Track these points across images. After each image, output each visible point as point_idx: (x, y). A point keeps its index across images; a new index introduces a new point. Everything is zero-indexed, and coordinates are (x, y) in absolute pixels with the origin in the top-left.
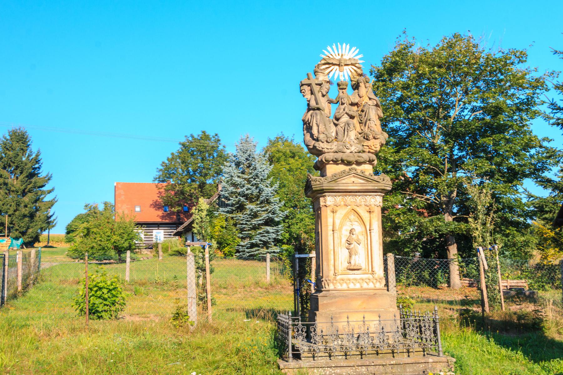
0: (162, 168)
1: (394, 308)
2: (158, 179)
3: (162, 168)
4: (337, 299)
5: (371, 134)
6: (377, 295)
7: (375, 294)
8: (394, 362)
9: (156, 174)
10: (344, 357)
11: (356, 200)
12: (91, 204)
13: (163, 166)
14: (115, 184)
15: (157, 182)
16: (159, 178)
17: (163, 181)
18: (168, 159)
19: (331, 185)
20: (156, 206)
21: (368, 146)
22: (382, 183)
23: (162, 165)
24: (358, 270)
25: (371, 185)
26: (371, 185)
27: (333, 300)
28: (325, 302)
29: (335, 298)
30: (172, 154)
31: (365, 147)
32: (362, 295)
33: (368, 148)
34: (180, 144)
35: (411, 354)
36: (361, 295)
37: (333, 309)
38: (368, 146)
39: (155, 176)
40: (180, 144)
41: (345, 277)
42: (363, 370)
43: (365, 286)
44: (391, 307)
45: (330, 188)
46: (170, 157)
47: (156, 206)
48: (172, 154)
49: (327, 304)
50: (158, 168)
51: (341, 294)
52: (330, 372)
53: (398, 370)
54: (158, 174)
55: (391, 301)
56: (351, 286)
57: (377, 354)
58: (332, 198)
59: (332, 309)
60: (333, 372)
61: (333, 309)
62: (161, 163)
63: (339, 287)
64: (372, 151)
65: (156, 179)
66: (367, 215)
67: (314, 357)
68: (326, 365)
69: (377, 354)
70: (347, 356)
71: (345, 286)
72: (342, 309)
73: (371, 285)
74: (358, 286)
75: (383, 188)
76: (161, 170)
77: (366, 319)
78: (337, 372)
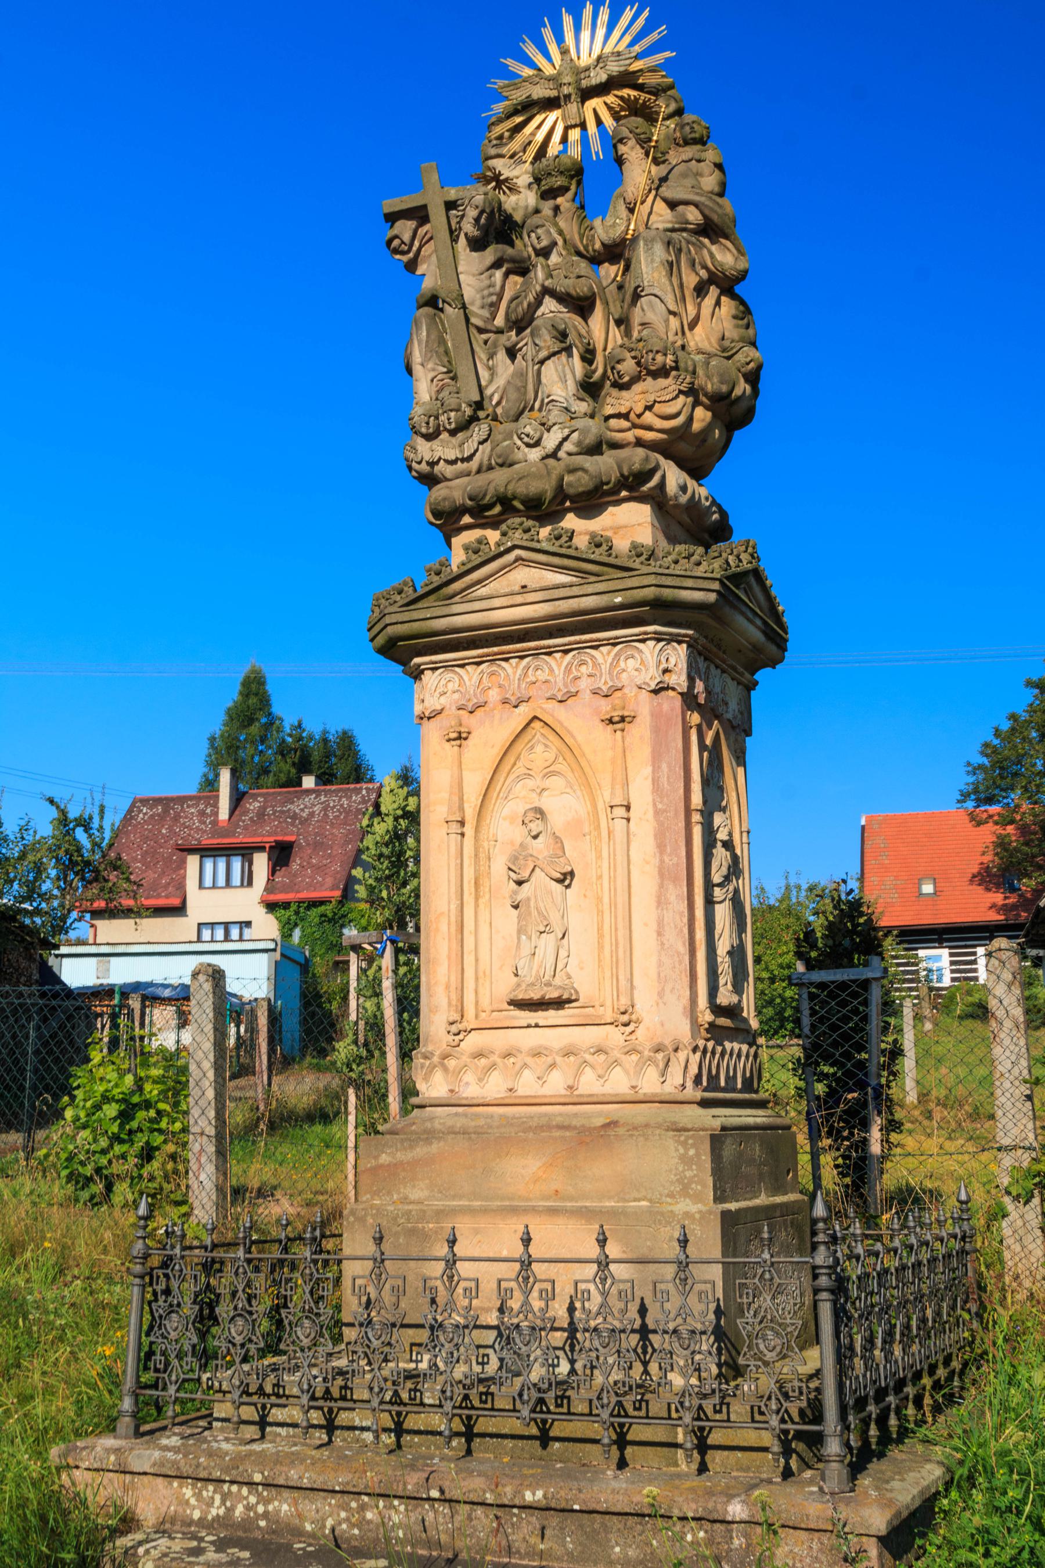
0: (985, 761)
1: (697, 1198)
2: (973, 797)
3: (985, 761)
4: (435, 1148)
5: (628, 355)
6: (621, 1131)
7: (612, 1124)
8: (539, 1494)
9: (964, 780)
10: (388, 1439)
11: (552, 670)
12: (823, 883)
13: (987, 756)
14: (863, 822)
15: (970, 804)
16: (976, 791)
17: (990, 800)
18: (997, 733)
19: (415, 615)
20: (986, 878)
21: (626, 416)
22: (645, 569)
23: (983, 754)
24: (559, 1003)
25: (590, 589)
26: (590, 589)
27: (420, 1151)
28: (384, 1159)
29: (428, 1141)
30: (1013, 717)
31: (613, 422)
32: (549, 1127)
33: (625, 424)
34: (1029, 684)
35: (716, 1459)
36: (546, 1126)
37: (417, 1192)
38: (626, 416)
39: (963, 787)
40: (1029, 684)
41: (497, 1040)
42: (396, 1519)
43: (589, 1083)
44: (685, 1192)
45: (416, 625)
46: (1006, 726)
47: (986, 878)
48: (1013, 717)
49: (393, 1169)
50: (969, 764)
51: (459, 1123)
52: (248, 1508)
53: (564, 1544)
54: (971, 779)
55: (684, 1159)
56: (528, 1085)
57: (545, 1439)
58: (449, 675)
59: (415, 1194)
60: (261, 1509)
61: (417, 1192)
62: (978, 747)
63: (471, 1090)
64: (649, 436)
65: (965, 796)
66: (604, 735)
67: (263, 1423)
68: (226, 1470)
69: (545, 1439)
70: (407, 1438)
71: (495, 1087)
72: (454, 1197)
73: (618, 1083)
74: (556, 1084)
75: (649, 593)
76: (981, 767)
77: (459, 1250)
78: (278, 1511)
